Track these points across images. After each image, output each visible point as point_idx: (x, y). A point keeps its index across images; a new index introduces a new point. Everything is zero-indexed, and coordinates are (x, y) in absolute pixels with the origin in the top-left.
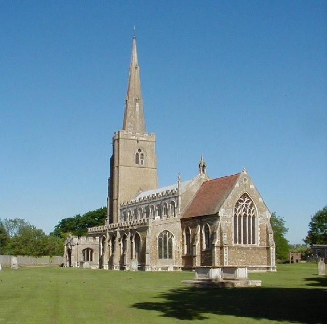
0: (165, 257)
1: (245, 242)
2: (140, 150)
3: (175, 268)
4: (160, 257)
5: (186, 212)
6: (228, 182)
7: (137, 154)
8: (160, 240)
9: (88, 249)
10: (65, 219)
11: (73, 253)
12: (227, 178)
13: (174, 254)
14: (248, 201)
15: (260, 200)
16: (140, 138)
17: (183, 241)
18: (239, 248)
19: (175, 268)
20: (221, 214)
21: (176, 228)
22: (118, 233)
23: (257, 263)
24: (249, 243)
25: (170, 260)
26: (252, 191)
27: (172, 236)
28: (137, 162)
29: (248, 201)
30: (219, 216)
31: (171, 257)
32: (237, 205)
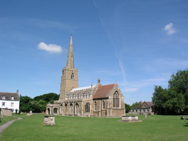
0: (88, 112)
1: (116, 107)
2: (73, 74)
3: (91, 116)
4: (86, 112)
5: (96, 93)
6: (111, 86)
7: (72, 75)
8: (86, 106)
9: (55, 108)
10: (157, 114)
11: (50, 110)
12: (111, 85)
13: (90, 111)
14: (117, 93)
15: (121, 93)
16: (73, 70)
17: (94, 106)
18: (115, 109)
19: (91, 116)
20: (109, 98)
21: (92, 102)
22: (39, 102)
23: (120, 114)
24: (118, 107)
25: (89, 113)
26: (119, 90)
27: (90, 105)
28: (72, 78)
29: (117, 93)
30: (169, 82)
31: (89, 112)
32: (114, 95)
